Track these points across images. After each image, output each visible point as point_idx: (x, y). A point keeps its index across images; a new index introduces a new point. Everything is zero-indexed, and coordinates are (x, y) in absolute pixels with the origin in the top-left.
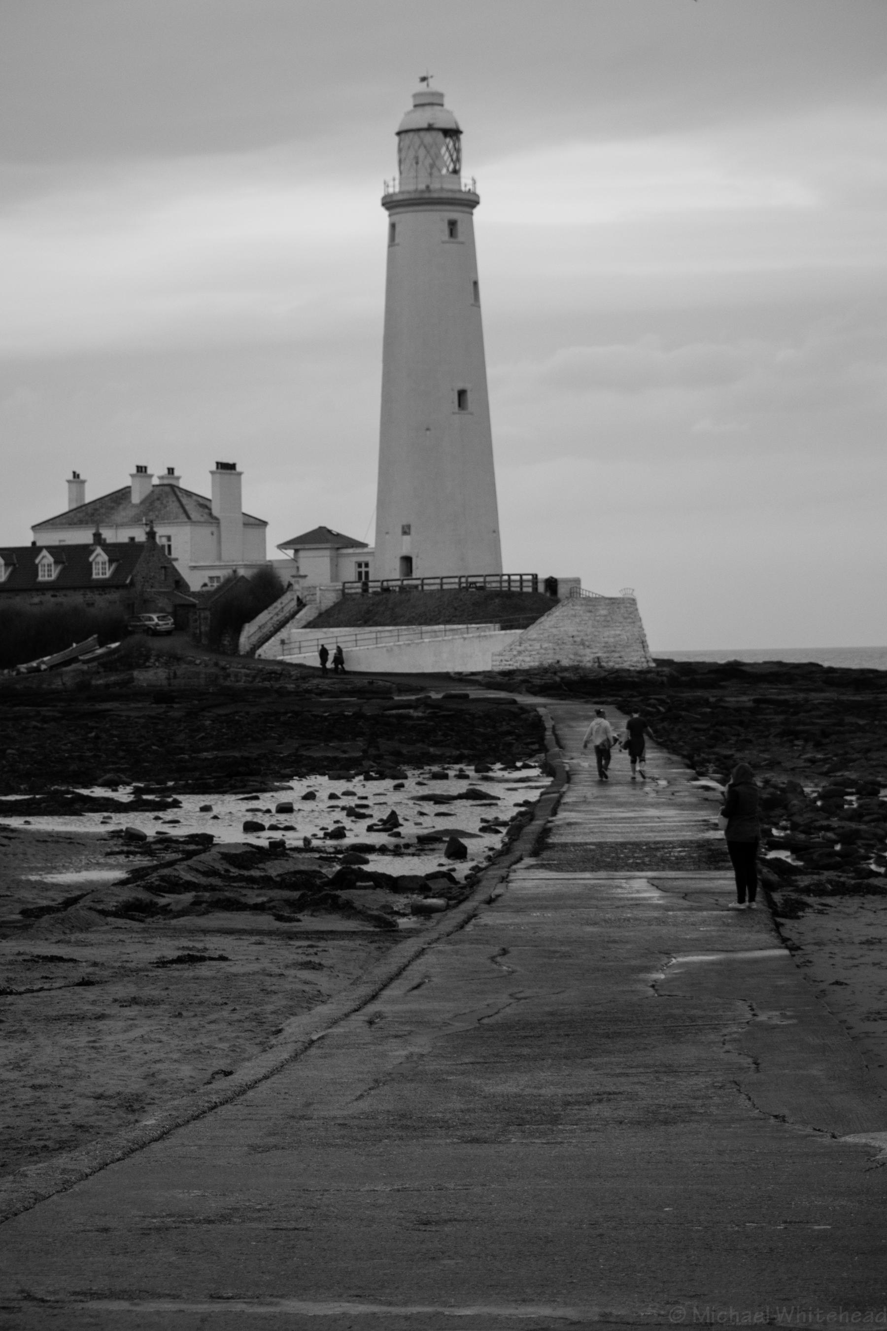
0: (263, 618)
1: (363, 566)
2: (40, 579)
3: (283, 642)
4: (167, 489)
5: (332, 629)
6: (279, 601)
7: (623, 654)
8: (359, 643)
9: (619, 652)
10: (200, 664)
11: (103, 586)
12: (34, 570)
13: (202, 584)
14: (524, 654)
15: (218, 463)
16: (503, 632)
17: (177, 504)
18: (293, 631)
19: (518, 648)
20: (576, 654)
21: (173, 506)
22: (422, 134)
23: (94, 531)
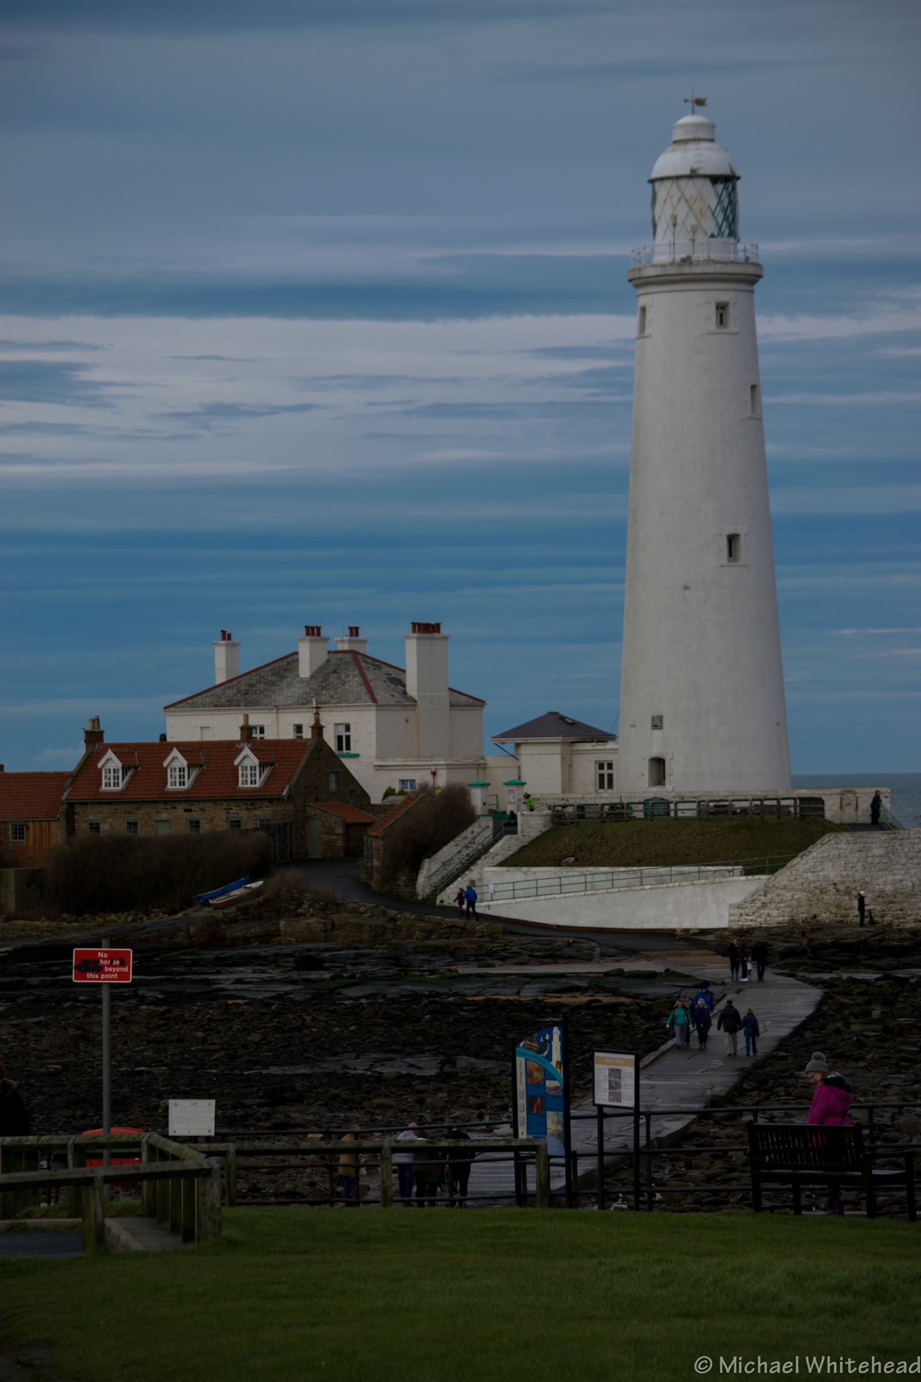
0: (448, 851)
1: (606, 767)
2: (169, 786)
4: (349, 657)
5: (533, 869)
6: (470, 829)
8: (564, 889)
9: (899, 903)
10: (365, 912)
11: (251, 799)
12: (162, 775)
13: (383, 791)
14: (771, 906)
15: (414, 624)
16: (744, 878)
17: (359, 679)
19: (763, 898)
20: (838, 906)
21: (354, 682)
22: (683, 183)
23: (241, 722)
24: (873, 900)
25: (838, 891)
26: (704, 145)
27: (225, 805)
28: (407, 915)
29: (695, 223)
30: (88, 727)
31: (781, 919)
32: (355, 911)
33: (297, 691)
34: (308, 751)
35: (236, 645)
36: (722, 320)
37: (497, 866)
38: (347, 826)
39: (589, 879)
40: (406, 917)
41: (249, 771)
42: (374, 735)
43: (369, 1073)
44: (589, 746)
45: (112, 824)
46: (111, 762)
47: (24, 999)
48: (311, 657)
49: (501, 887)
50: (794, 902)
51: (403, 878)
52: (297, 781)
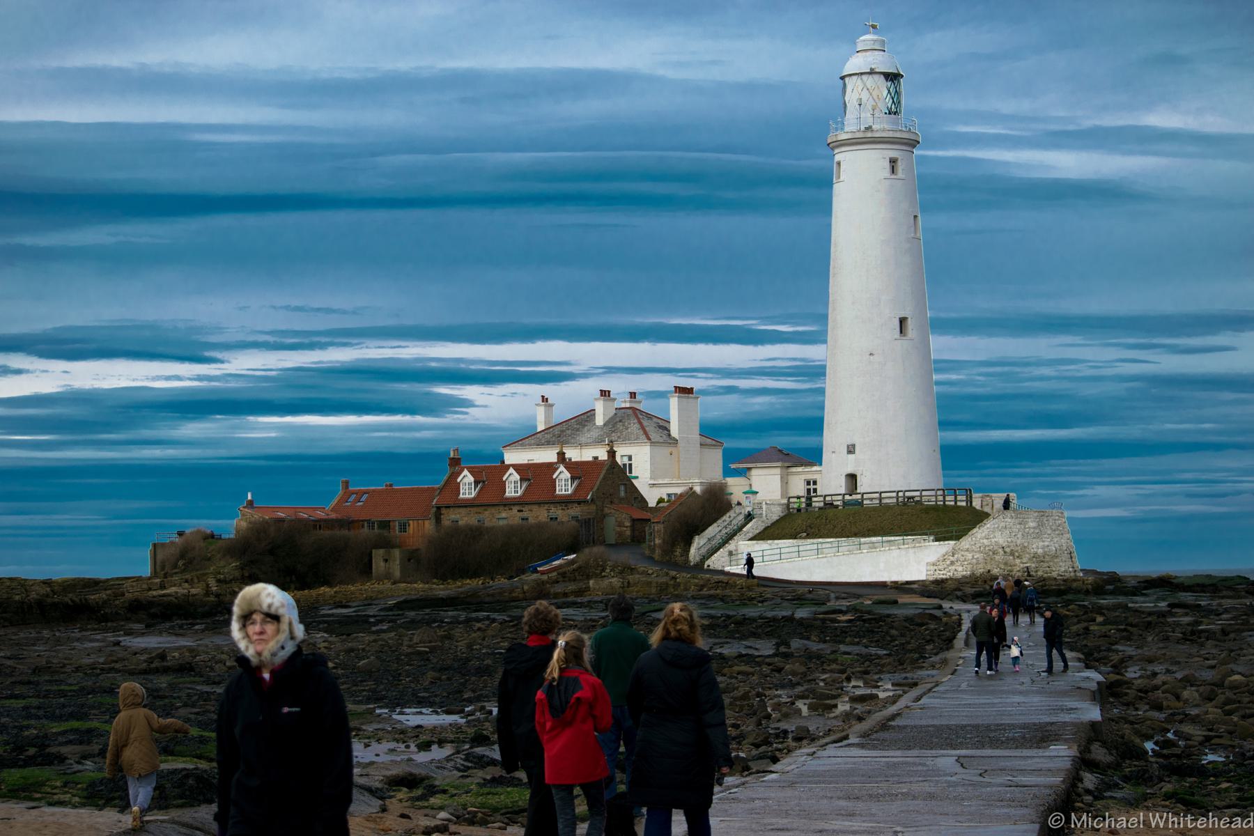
0: (712, 530)
3: (731, 553)
11: (565, 502)
12: (502, 486)
17: (637, 426)
18: (743, 546)
20: (1006, 564)
21: (634, 427)
22: (865, 77)
33: (595, 434)
35: (552, 406)
36: (893, 170)
40: (682, 577)
41: (564, 483)
44: (800, 469)
45: (465, 519)
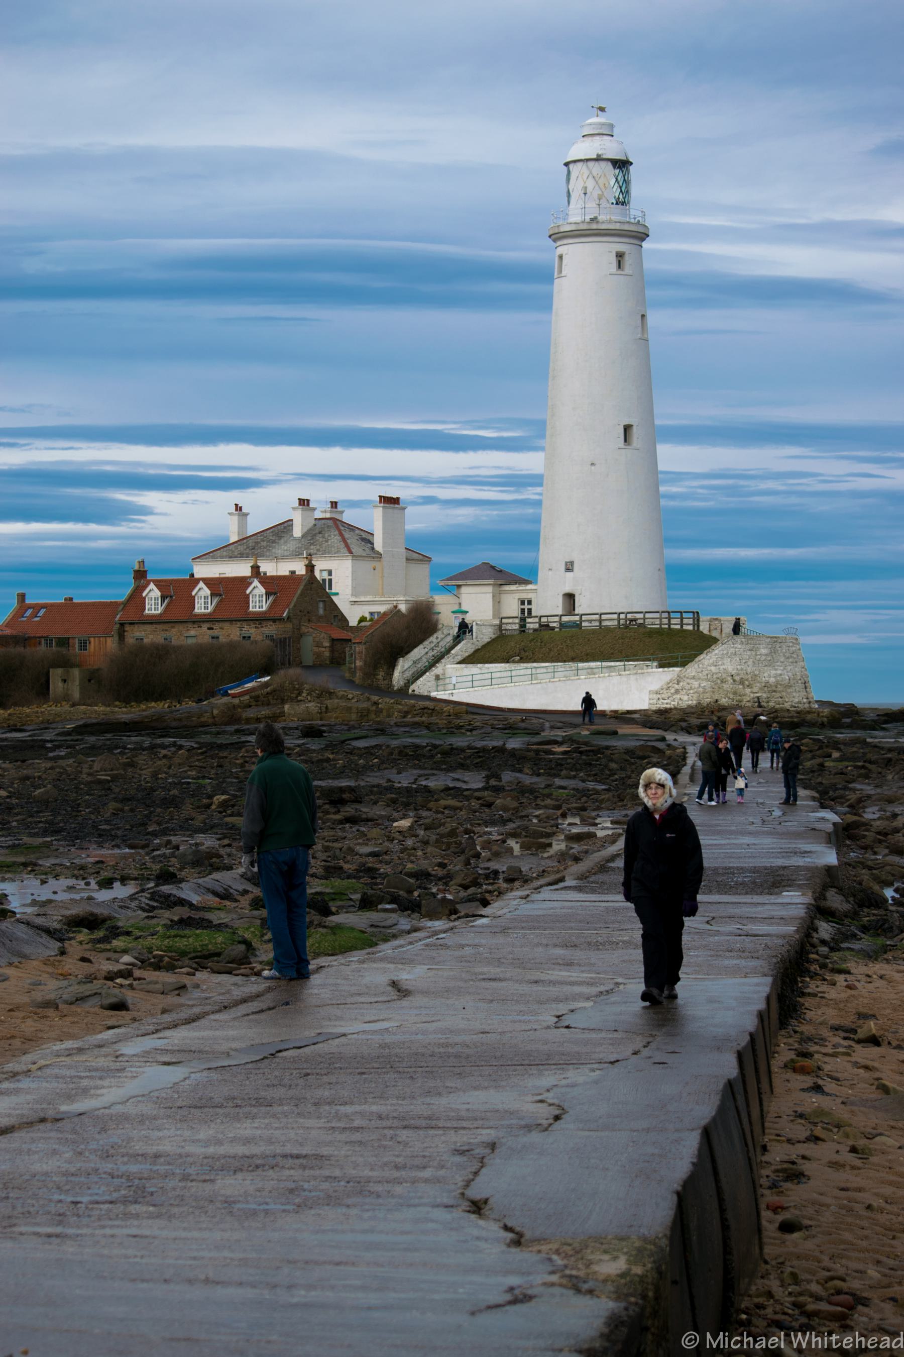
0: (418, 652)
3: (437, 678)
4: (330, 523)
5: (487, 665)
6: (435, 636)
7: (784, 694)
9: (780, 692)
11: (259, 619)
14: (682, 692)
16: (661, 670)
20: (735, 693)
21: (335, 539)
22: (591, 164)
24: (761, 689)
25: (734, 681)
26: (606, 138)
27: (239, 624)
28: (387, 700)
29: (600, 193)
30: (136, 567)
31: (690, 702)
32: (345, 698)
33: (292, 546)
34: (304, 584)
35: (247, 514)
36: (620, 265)
37: (458, 663)
38: (333, 641)
39: (534, 671)
40: (385, 702)
41: (258, 599)
42: (350, 579)
43: (414, 786)
44: (513, 587)
45: (150, 636)
46: (152, 593)
47: (81, 747)
48: (302, 522)
49: (460, 679)
50: (701, 689)
51: (382, 673)
52: (295, 606)
